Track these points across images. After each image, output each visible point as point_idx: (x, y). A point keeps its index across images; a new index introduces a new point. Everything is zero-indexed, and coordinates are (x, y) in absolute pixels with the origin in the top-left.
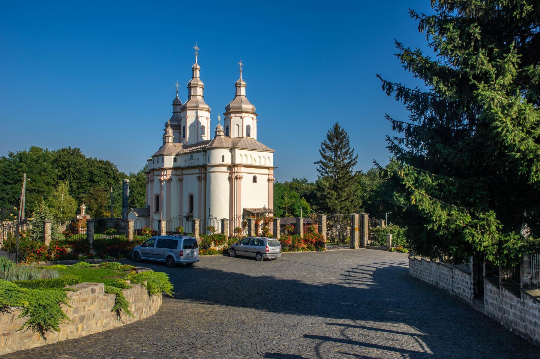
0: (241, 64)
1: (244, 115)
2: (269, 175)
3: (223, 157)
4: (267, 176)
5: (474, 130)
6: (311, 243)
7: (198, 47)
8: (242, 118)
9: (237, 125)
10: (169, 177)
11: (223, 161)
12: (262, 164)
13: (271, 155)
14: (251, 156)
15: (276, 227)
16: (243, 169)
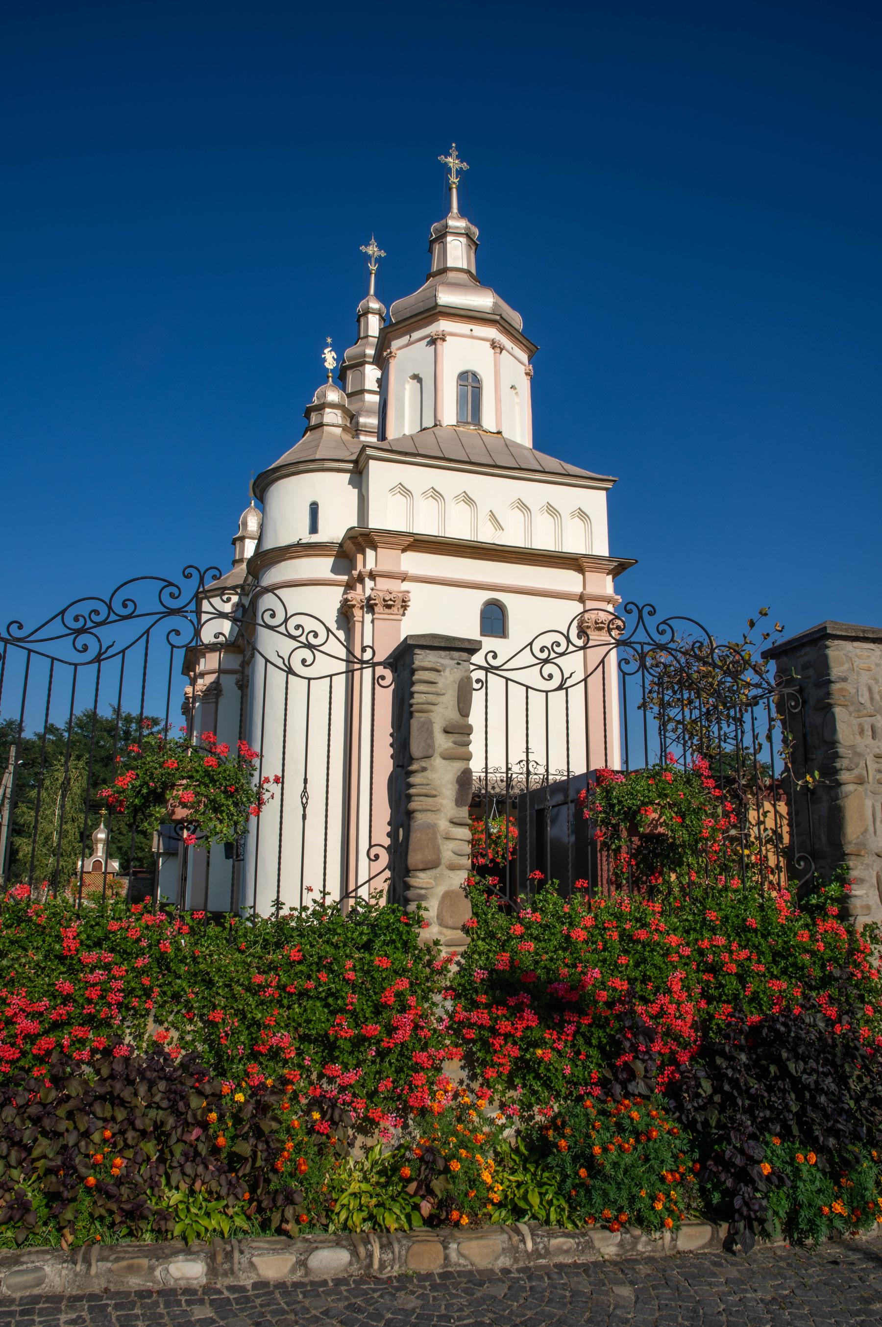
0: (452, 162)
1: (444, 325)
2: (581, 599)
3: (314, 509)
4: (578, 608)
5: (726, 1068)
6: (618, 1043)
7: (380, 248)
8: (433, 342)
9: (417, 378)
10: (210, 679)
11: (314, 529)
12: (544, 542)
13: (596, 502)
14: (469, 500)
15: (525, 850)
16: (414, 562)
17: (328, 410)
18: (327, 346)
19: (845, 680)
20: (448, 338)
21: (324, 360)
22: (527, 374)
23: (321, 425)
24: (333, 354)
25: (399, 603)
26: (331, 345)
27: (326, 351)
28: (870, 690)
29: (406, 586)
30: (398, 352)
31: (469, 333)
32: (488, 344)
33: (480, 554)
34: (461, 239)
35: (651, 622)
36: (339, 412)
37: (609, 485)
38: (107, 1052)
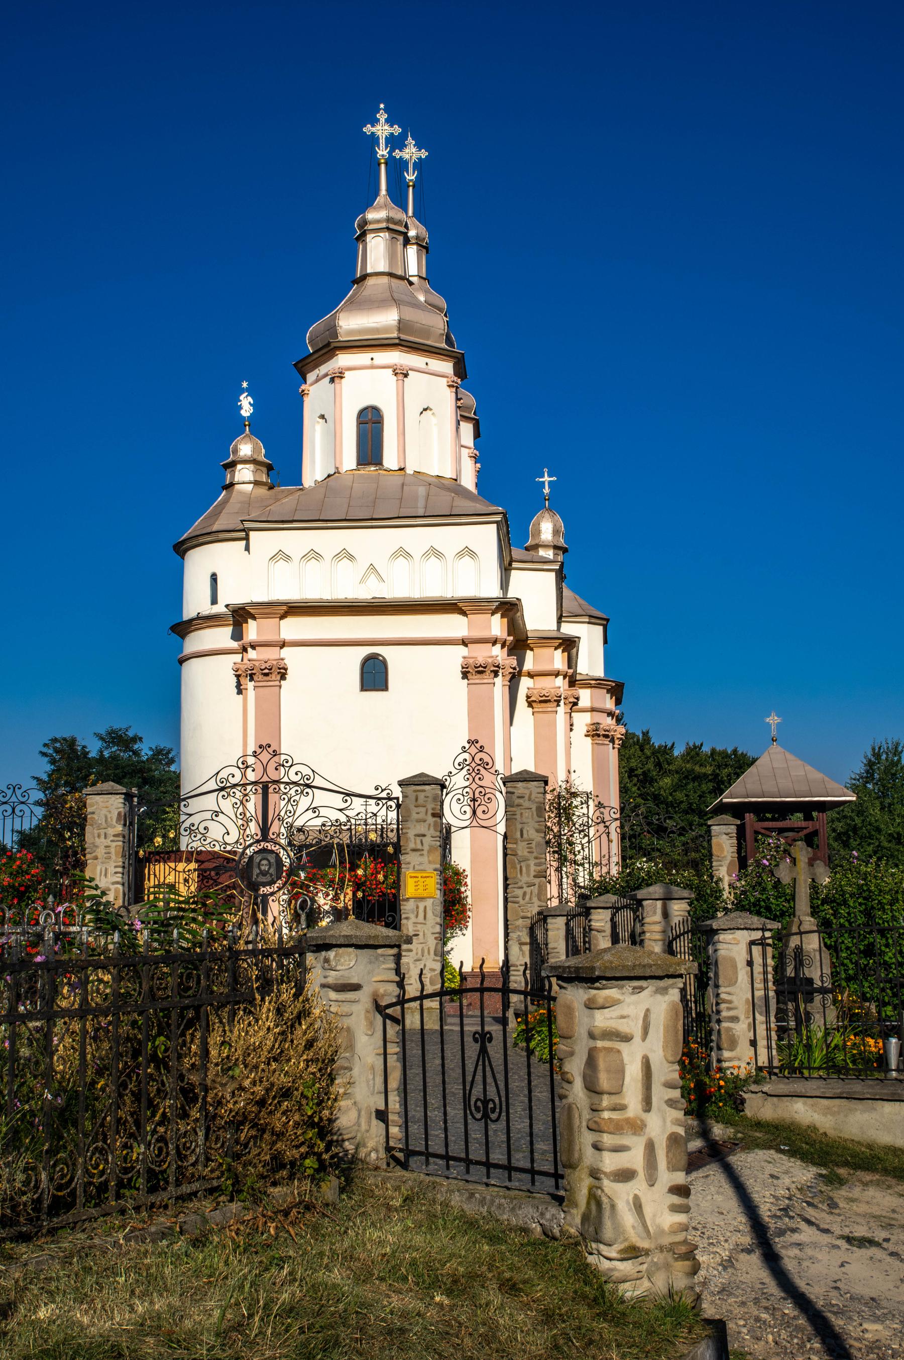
1: (343, 360)
3: (214, 578)
7: (419, 146)
11: (214, 601)
17: (239, 467)
18: (242, 391)
19: (93, 813)
20: (347, 374)
21: (241, 408)
22: (449, 386)
23: (232, 485)
24: (250, 399)
25: (275, 671)
26: (247, 390)
27: (242, 398)
28: (106, 817)
29: (286, 652)
30: (311, 388)
31: (369, 362)
32: (390, 371)
33: (358, 611)
34: (382, 234)
35: (19, 792)
36: (251, 467)
37: (498, 518)
38: (579, 1328)
